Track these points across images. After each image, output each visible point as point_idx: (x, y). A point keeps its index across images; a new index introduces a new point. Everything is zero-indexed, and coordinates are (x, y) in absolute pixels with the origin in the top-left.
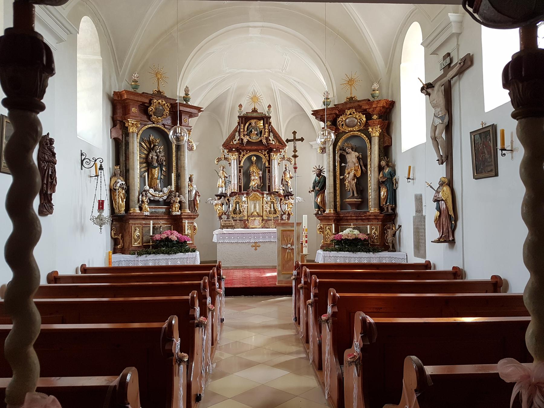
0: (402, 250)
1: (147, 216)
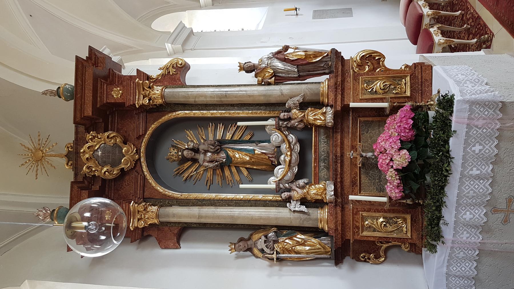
1: (335, 190)
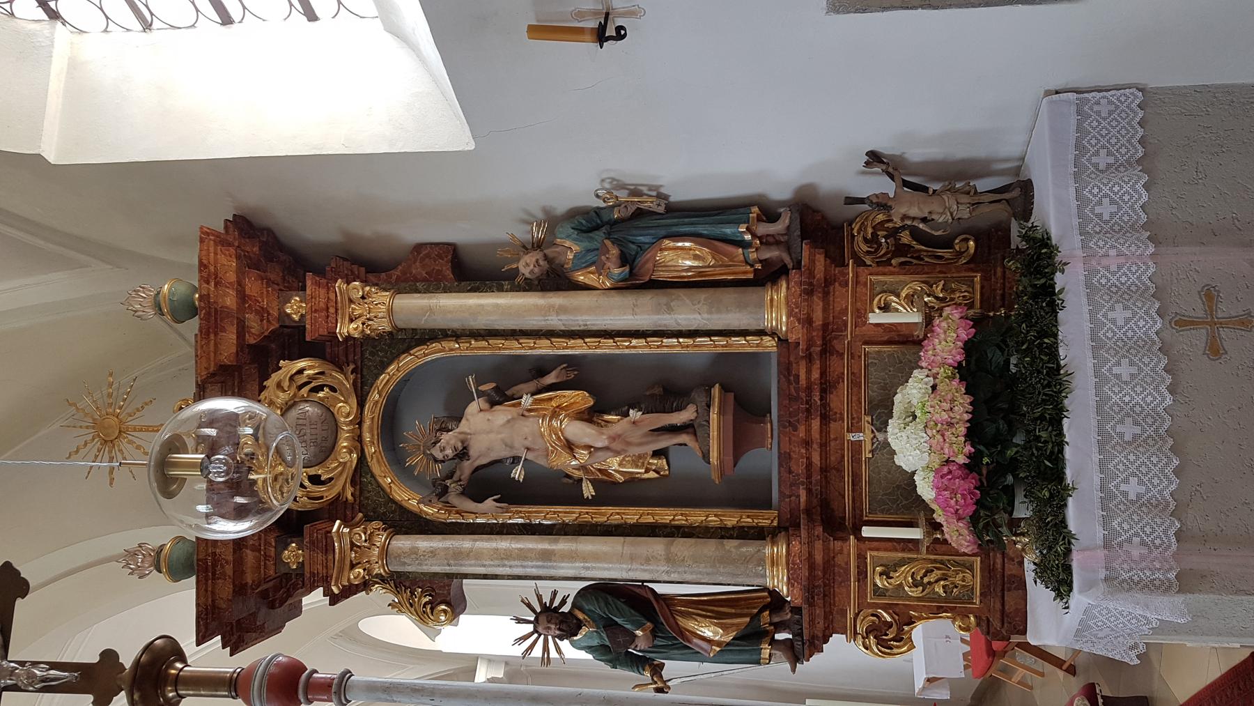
0: (1008, 148)
